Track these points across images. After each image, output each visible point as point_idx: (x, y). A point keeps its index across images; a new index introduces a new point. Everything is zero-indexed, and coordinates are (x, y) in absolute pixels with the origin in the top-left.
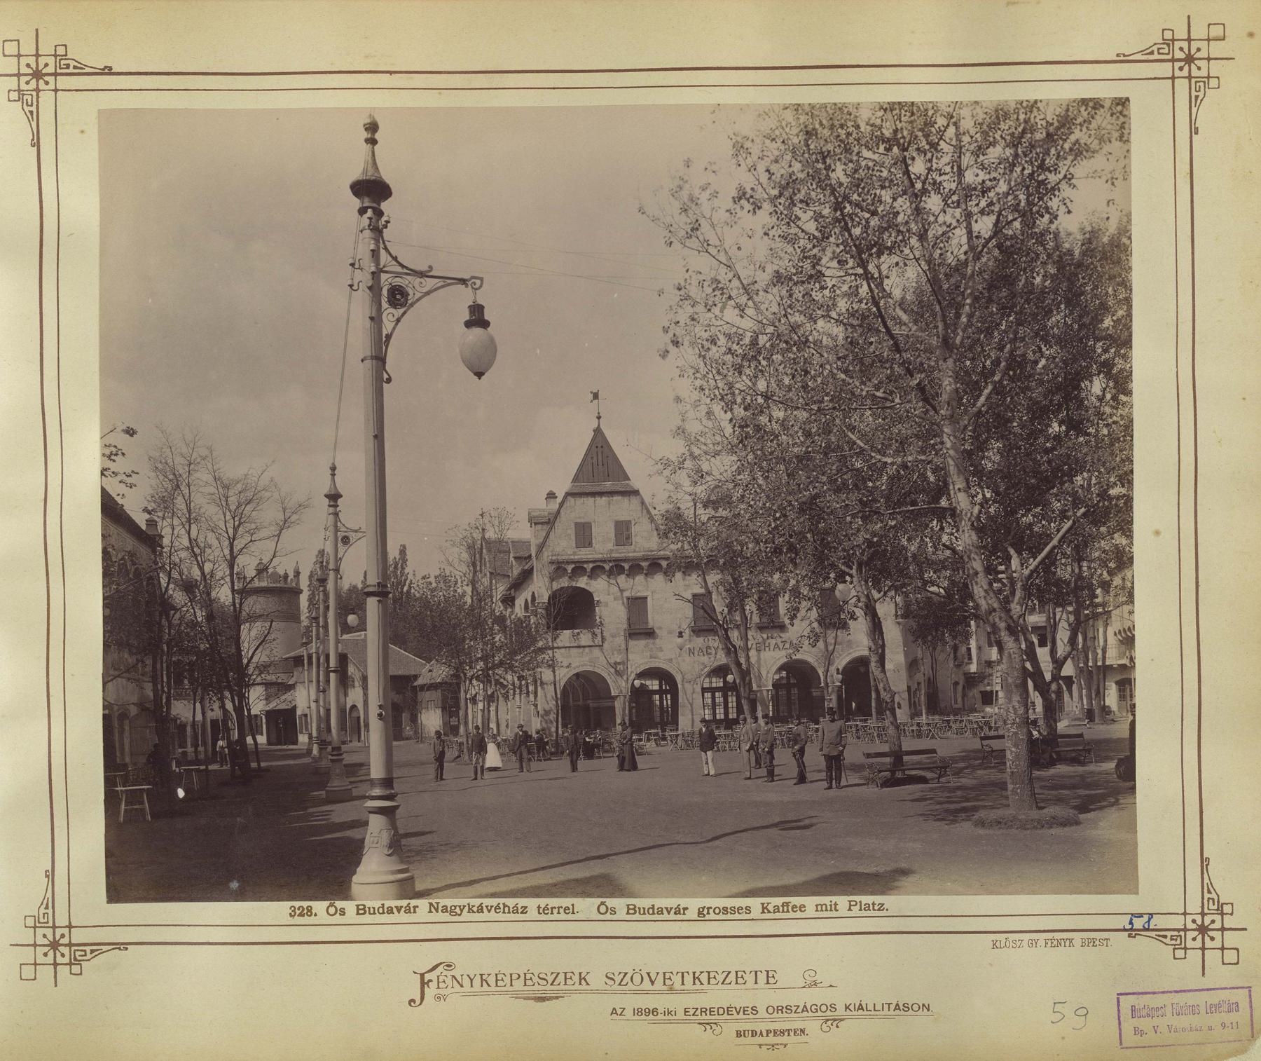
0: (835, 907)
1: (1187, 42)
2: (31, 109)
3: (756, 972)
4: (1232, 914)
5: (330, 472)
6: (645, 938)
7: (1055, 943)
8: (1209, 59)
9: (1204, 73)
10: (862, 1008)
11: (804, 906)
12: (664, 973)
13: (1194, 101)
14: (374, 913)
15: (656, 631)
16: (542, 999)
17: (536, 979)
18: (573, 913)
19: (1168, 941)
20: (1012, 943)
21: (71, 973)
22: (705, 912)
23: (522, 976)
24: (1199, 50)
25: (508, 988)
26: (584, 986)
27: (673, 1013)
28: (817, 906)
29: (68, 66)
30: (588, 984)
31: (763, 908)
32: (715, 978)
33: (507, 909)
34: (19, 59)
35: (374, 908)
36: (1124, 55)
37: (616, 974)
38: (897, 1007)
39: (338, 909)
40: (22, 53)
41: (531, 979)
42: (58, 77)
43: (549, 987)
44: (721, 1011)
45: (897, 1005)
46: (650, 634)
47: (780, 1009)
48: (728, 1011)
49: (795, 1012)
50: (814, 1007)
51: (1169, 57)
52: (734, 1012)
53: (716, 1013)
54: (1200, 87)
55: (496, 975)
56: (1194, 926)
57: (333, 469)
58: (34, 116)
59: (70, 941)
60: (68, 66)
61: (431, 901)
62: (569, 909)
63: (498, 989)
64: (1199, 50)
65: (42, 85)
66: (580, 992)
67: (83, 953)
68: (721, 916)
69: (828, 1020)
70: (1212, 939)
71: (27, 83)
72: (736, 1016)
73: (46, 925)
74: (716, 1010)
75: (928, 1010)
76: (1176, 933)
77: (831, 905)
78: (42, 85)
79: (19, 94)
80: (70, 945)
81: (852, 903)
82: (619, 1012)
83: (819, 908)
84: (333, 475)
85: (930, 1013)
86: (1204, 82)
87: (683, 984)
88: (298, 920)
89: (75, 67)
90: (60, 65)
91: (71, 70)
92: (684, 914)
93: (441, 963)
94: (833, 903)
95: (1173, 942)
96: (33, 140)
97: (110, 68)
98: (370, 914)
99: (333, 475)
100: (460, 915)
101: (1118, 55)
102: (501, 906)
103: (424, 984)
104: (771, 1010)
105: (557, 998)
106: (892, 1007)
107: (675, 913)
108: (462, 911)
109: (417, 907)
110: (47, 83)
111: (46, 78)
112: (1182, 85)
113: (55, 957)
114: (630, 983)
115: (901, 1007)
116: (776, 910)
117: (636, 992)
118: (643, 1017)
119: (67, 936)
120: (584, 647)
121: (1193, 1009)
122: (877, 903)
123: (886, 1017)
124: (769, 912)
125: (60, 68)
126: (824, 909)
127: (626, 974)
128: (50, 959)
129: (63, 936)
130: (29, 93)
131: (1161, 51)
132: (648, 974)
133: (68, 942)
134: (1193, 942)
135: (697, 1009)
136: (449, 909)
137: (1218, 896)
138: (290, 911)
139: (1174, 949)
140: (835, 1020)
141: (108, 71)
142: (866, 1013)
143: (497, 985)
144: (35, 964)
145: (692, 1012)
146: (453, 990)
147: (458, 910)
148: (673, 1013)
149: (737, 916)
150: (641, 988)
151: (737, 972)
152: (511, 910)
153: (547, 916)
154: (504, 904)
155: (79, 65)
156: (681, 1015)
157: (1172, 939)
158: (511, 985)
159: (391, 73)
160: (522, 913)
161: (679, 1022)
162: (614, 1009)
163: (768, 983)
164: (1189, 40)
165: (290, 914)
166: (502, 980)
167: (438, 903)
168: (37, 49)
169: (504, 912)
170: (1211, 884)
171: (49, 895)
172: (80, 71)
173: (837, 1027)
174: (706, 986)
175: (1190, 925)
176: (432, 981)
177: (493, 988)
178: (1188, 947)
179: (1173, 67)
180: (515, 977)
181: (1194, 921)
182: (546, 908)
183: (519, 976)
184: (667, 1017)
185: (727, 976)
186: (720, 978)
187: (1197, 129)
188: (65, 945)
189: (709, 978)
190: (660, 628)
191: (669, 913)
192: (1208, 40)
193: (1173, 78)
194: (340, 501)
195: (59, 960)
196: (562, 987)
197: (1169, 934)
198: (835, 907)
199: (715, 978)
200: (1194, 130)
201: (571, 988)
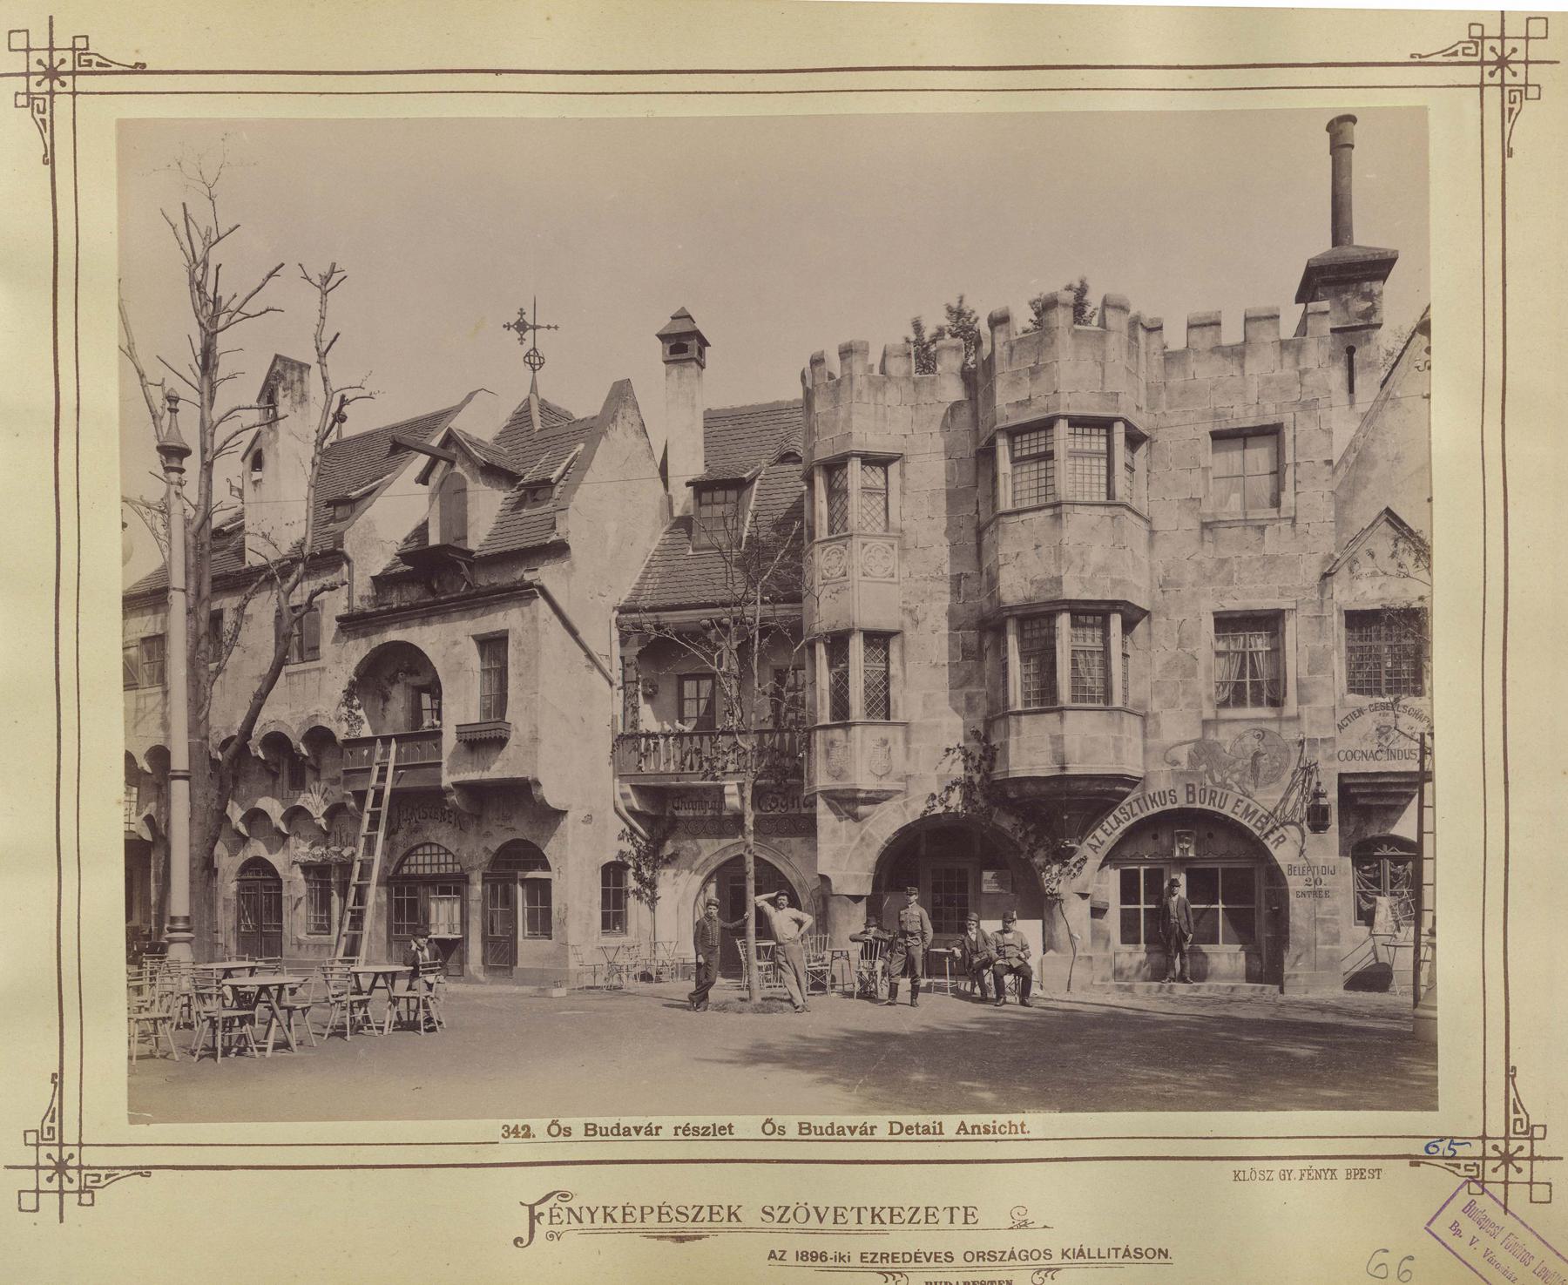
0: (730, 1130)
1: (1499, 41)
3: (952, 1209)
6: (862, 1162)
7: (1314, 1174)
8: (1527, 62)
9: (1520, 80)
10: (1083, 1255)
12: (927, 1208)
16: (680, 1239)
17: (673, 1214)
20: (1258, 1175)
23: (656, 1210)
24: (1514, 50)
25: (639, 1224)
26: (734, 1223)
27: (846, 1259)
28: (676, 1128)
30: (739, 1220)
33: (1013, 1128)
34: (69, 49)
35: (821, 1127)
36: (1420, 56)
37: (776, 1208)
38: (1127, 1253)
39: (905, 1125)
41: (668, 1214)
43: (690, 1224)
44: (907, 1258)
45: (1127, 1250)
47: (980, 1256)
48: (916, 1257)
49: (1001, 1260)
50: (1023, 1253)
51: (1477, 59)
52: (923, 1259)
53: (900, 1259)
54: (1515, 97)
55: (624, 1208)
56: (65, 1157)
58: (47, 126)
60: (90, 62)
63: (626, 1225)
64: (1514, 50)
65: (56, 84)
66: (730, 1230)
69: (1040, 1270)
70: (1519, 1170)
71: (39, 84)
72: (925, 1264)
74: (900, 1256)
75: (1166, 1256)
76: (1471, 1162)
77: (934, 1127)
78: (57, 86)
79: (28, 98)
81: (589, 1127)
82: (778, 1256)
85: (1168, 1260)
86: (1521, 91)
87: (859, 1222)
90: (79, 62)
93: (554, 1193)
96: (46, 155)
101: (1412, 56)
103: (534, 1218)
104: (969, 1257)
105: (700, 1238)
106: (1121, 1253)
109: (661, 1127)
111: (62, 78)
113: (1523, 1159)
115: (1132, 1253)
118: (809, 1263)
121: (1526, 1259)
122: (921, 1125)
123: (1111, 1266)
127: (787, 1208)
128: (1525, 1165)
131: (1467, 51)
133: (77, 1164)
135: (876, 1254)
137: (1528, 1116)
140: (1050, 1270)
141: (139, 69)
142: (1087, 1260)
143: (624, 1221)
145: (870, 1257)
146: (571, 1227)
148: (846, 1259)
150: (807, 1226)
154: (1010, 1122)
155: (104, 62)
156: (856, 1261)
157: (49, 1128)
158: (642, 1221)
161: (853, 1270)
162: (773, 1252)
163: (966, 1222)
164: (1502, 38)
165: (503, 1135)
166: (631, 1214)
171: (1508, 126)
172: (55, 1113)
173: (1053, 1278)
174: (888, 1226)
177: (619, 1225)
179: (1482, 72)
180: (647, 1210)
183: (652, 1211)
184: (837, 1264)
186: (907, 1215)
188: (1507, 1145)
191: (852, 1133)
193: (1482, 86)
198: (730, 1130)
200: (1507, 152)
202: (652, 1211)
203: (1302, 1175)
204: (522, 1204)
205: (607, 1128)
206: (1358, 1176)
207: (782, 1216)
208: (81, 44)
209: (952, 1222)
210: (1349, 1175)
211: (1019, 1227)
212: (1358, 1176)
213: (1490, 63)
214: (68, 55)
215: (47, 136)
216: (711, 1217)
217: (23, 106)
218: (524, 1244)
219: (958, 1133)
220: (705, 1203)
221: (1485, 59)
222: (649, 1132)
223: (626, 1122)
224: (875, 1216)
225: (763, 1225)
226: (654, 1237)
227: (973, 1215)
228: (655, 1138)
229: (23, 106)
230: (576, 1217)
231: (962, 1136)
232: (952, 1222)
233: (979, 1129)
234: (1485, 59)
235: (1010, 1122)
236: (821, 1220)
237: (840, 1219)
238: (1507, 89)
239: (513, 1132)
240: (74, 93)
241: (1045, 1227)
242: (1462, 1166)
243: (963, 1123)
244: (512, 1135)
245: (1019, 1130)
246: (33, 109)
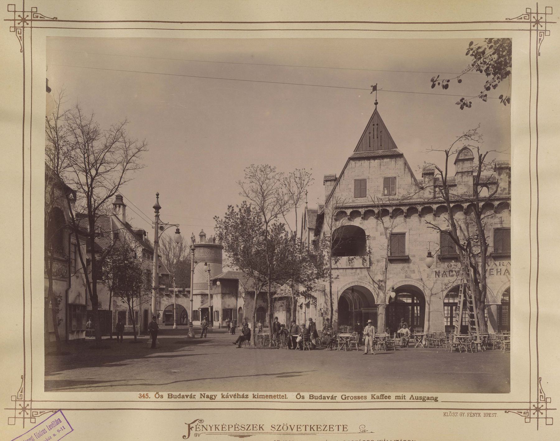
2: (20, 35)
3: (338, 426)
4: (550, 402)
5: (156, 196)
7: (472, 415)
8: (546, 22)
11: (390, 397)
12: (297, 426)
13: (539, 41)
14: (176, 398)
15: (411, 258)
17: (240, 428)
18: (286, 398)
19: (522, 414)
21: (31, 422)
22: (426, 399)
23: (234, 426)
25: (227, 431)
28: (396, 397)
29: (37, 17)
30: (263, 430)
31: (372, 397)
32: (320, 428)
33: (239, 396)
35: (176, 395)
36: (509, 19)
37: (276, 426)
40: (16, 10)
41: (238, 427)
42: (33, 22)
43: (245, 431)
46: (406, 260)
51: (529, 20)
55: (222, 425)
56: (534, 408)
57: (158, 195)
58: (540, 391)
59: (31, 407)
60: (37, 17)
61: (201, 393)
62: (284, 396)
63: (222, 432)
65: (25, 25)
66: (259, 433)
67: (37, 413)
68: (354, 400)
73: (21, 400)
76: (526, 411)
77: (402, 397)
78: (25, 25)
80: (31, 409)
81: (170, 395)
83: (397, 398)
84: (158, 198)
86: (543, 33)
87: (306, 430)
88: (142, 399)
89: (41, 17)
91: (39, 19)
92: (194, 398)
94: (403, 396)
95: (525, 415)
96: (21, 49)
97: (56, 18)
98: (174, 398)
99: (158, 198)
100: (214, 399)
101: (506, 19)
102: (237, 395)
103: (190, 429)
105: (249, 436)
107: (331, 399)
108: (215, 397)
109: (336, 397)
110: (28, 24)
111: (27, 22)
112: (534, 33)
114: (282, 429)
116: (378, 398)
117: (284, 434)
119: (30, 405)
120: (356, 268)
122: (281, 395)
124: (375, 398)
125: (34, 18)
126: (399, 398)
127: (280, 426)
129: (28, 405)
130: (20, 28)
132: (290, 426)
134: (20, 403)
136: (209, 397)
138: (139, 396)
139: (525, 418)
141: (55, 19)
143: (222, 430)
144: (15, 418)
146: (202, 432)
147: (213, 397)
149: (360, 400)
151: (330, 426)
152: (241, 396)
153: (141, 399)
154: (238, 394)
155: (42, 17)
157: (524, 414)
158: (229, 430)
159: (181, 22)
160: (246, 398)
163: (343, 431)
164: (537, 13)
165: (139, 397)
167: (204, 394)
168: (24, 9)
169: (260, 398)
170: (542, 389)
171: (539, 45)
172: (43, 19)
174: (316, 432)
175: (532, 408)
176: (193, 427)
177: (221, 431)
178: (531, 417)
180: (230, 426)
181: (534, 406)
182: (235, 395)
183: (232, 426)
185: (326, 427)
186: (323, 428)
187: (539, 53)
188: (29, 409)
189: (317, 428)
190: (414, 256)
191: (328, 399)
192: (546, 14)
193: (530, 30)
194: (160, 210)
195: (26, 416)
196: (251, 431)
197: (523, 411)
199: (320, 428)
201: (256, 431)
202: (232, 426)
203: (468, 415)
204: (186, 424)
205: (317, 396)
206: (488, 416)
207: (278, 428)
208: (34, 10)
209: (338, 430)
210: (485, 415)
211: (362, 432)
212: (488, 416)
213: (533, 22)
214: (30, 14)
215: (22, 42)
216: (253, 429)
217: (13, 31)
218: (186, 438)
219: (410, 399)
220: (251, 424)
221: (532, 21)
222: (332, 398)
223: (324, 394)
224: (311, 428)
225: (272, 431)
226: (233, 436)
227: (346, 428)
228: (404, 400)
229: (13, 31)
230: (205, 428)
231: (412, 400)
232: (338, 430)
233: (272, 397)
234: (532, 21)
235: (238, 394)
236: (292, 430)
237: (299, 429)
238: (539, 32)
239: (143, 396)
240: (31, 27)
241: (372, 432)
242: (22, 394)
243: (412, 396)
244: (142, 398)
245: (403, 398)
246: (16, 32)
